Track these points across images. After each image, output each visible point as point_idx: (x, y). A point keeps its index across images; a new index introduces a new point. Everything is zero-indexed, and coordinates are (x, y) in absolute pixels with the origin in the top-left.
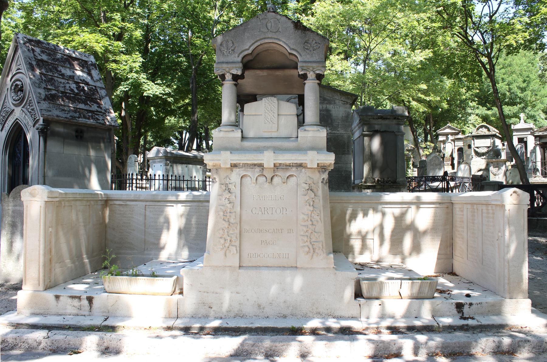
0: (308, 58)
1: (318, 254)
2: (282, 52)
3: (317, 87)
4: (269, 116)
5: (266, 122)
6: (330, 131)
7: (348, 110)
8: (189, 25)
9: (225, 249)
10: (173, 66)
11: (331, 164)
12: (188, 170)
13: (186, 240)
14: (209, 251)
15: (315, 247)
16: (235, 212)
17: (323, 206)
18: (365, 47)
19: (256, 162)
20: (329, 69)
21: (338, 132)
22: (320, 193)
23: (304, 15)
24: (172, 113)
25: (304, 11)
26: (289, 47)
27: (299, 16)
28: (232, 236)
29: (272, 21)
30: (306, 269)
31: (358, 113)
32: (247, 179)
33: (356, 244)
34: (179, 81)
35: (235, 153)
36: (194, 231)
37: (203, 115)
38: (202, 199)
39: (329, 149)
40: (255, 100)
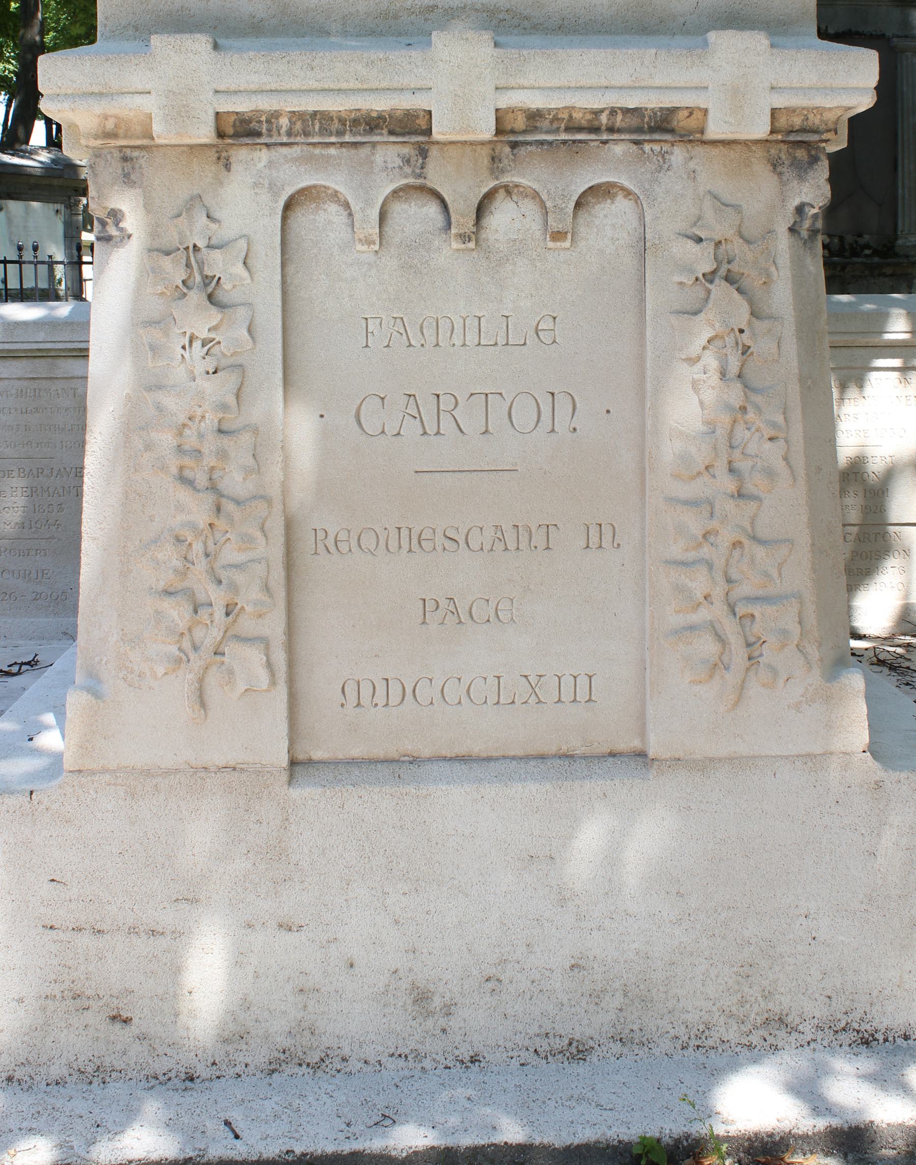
9: (197, 662)
17: (802, 380)
19: (379, 104)
22: (782, 296)
28: (240, 578)
30: (703, 765)
32: (321, 217)
35: (240, 50)
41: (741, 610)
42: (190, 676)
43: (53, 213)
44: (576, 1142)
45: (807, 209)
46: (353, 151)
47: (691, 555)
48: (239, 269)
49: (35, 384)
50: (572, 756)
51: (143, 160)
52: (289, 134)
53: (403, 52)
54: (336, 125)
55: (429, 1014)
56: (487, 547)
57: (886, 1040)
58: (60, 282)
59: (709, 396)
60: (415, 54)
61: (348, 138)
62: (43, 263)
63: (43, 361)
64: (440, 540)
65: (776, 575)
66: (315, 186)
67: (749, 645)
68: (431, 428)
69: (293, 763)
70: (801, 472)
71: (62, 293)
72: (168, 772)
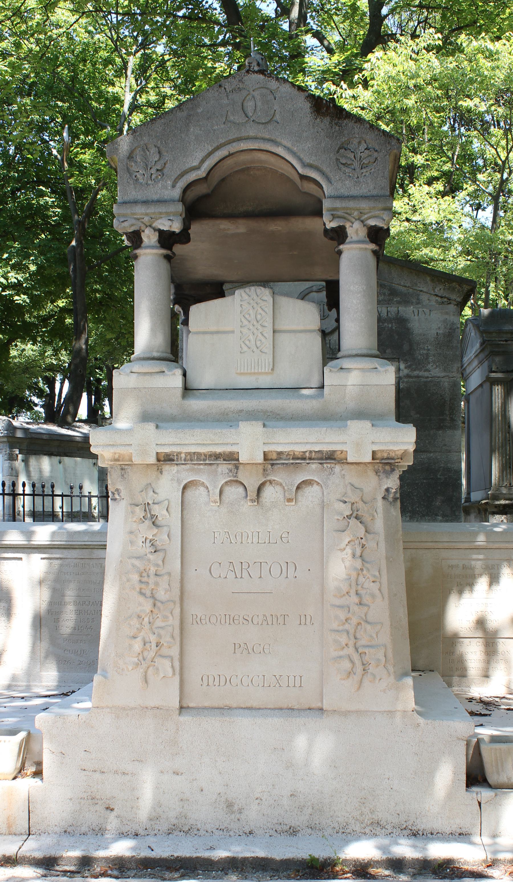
0: (346, 187)
1: (374, 676)
2: (282, 175)
3: (372, 261)
4: (249, 333)
5: (245, 349)
6: (406, 371)
7: (452, 318)
8: (64, 117)
9: (144, 665)
10: (27, 217)
11: (405, 452)
12: (65, 470)
13: (54, 641)
14: (104, 670)
15: (366, 658)
16: (169, 574)
17: (387, 558)
18: (496, 164)
19: (219, 450)
20: (408, 220)
21: (426, 374)
22: (379, 524)
23: (345, 86)
24: (27, 332)
25: (347, 74)
26: (300, 160)
27: (333, 88)
28: (162, 632)
29: (256, 94)
30: (346, 714)
31: (477, 327)
32: (197, 492)
33: (473, 653)
34: (41, 253)
35: (166, 429)
36: (69, 619)
37: (101, 336)
38: (86, 540)
39: (402, 416)
40: (221, 294)
41: (360, 650)
42: (141, 670)
43: (92, 465)
44: (285, 858)
45: (390, 490)
46: (210, 467)
47: (341, 628)
48: (165, 512)
49: (82, 561)
50: (293, 709)
51: (129, 469)
52: (185, 460)
53: (228, 430)
54: (203, 457)
55: (233, 812)
56: (260, 623)
57: (423, 834)
58: (95, 508)
59: (348, 564)
60: (233, 430)
61: (207, 462)
62: (85, 496)
63: (87, 550)
64: (241, 619)
65: (375, 637)
66: (195, 480)
67: (363, 664)
68: (239, 576)
69: (181, 708)
70: (386, 595)
71: (96, 515)
72: (132, 709)
